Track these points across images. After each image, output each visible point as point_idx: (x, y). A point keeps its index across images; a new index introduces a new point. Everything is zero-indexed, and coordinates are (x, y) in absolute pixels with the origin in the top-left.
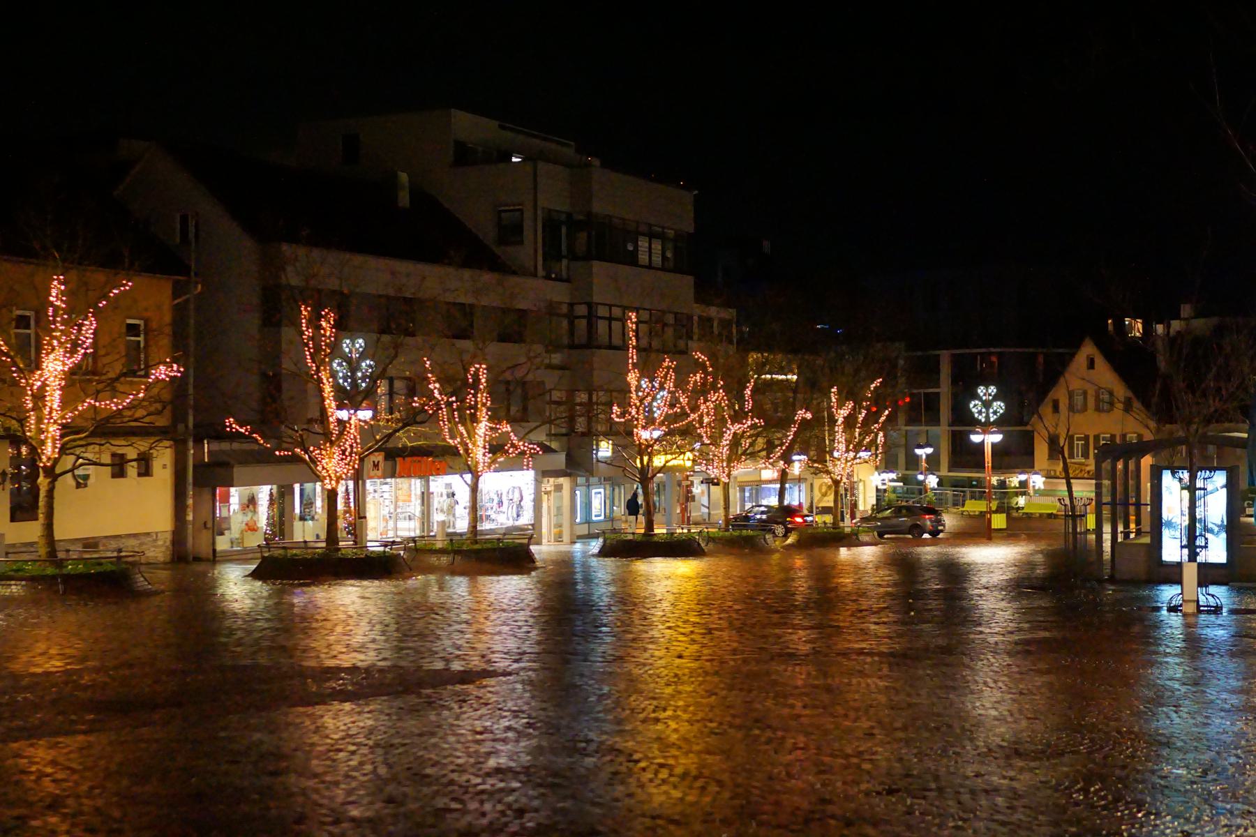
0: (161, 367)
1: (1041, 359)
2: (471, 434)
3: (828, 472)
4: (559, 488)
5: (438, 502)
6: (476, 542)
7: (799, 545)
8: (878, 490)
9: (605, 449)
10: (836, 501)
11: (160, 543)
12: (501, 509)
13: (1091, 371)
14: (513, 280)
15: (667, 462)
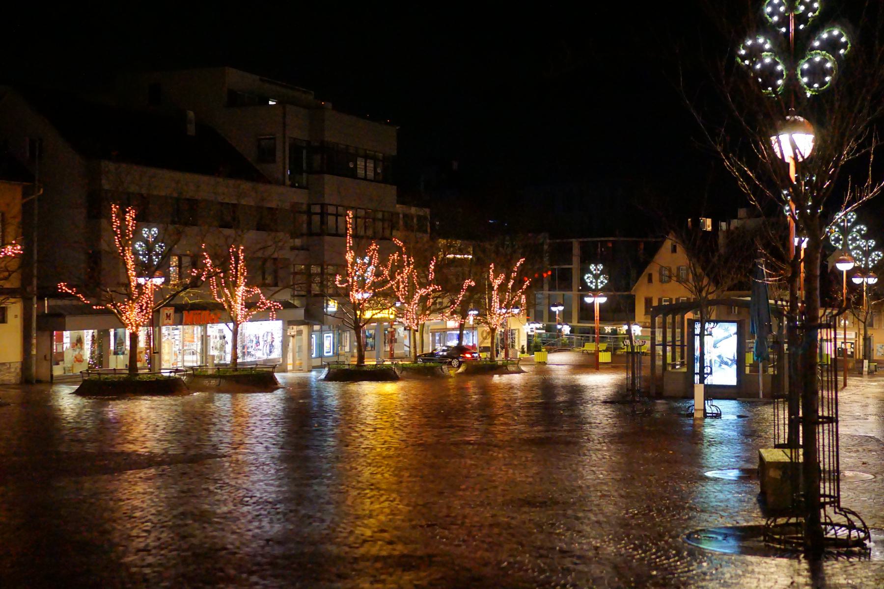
0: (9, 247)
1: (642, 246)
2: (233, 295)
3: (487, 323)
4: (300, 333)
5: (214, 342)
6: (236, 370)
7: (467, 373)
8: (529, 336)
9: (332, 306)
10: (492, 343)
11: (13, 370)
12: (258, 347)
13: (674, 254)
14: (261, 187)
15: (374, 315)
